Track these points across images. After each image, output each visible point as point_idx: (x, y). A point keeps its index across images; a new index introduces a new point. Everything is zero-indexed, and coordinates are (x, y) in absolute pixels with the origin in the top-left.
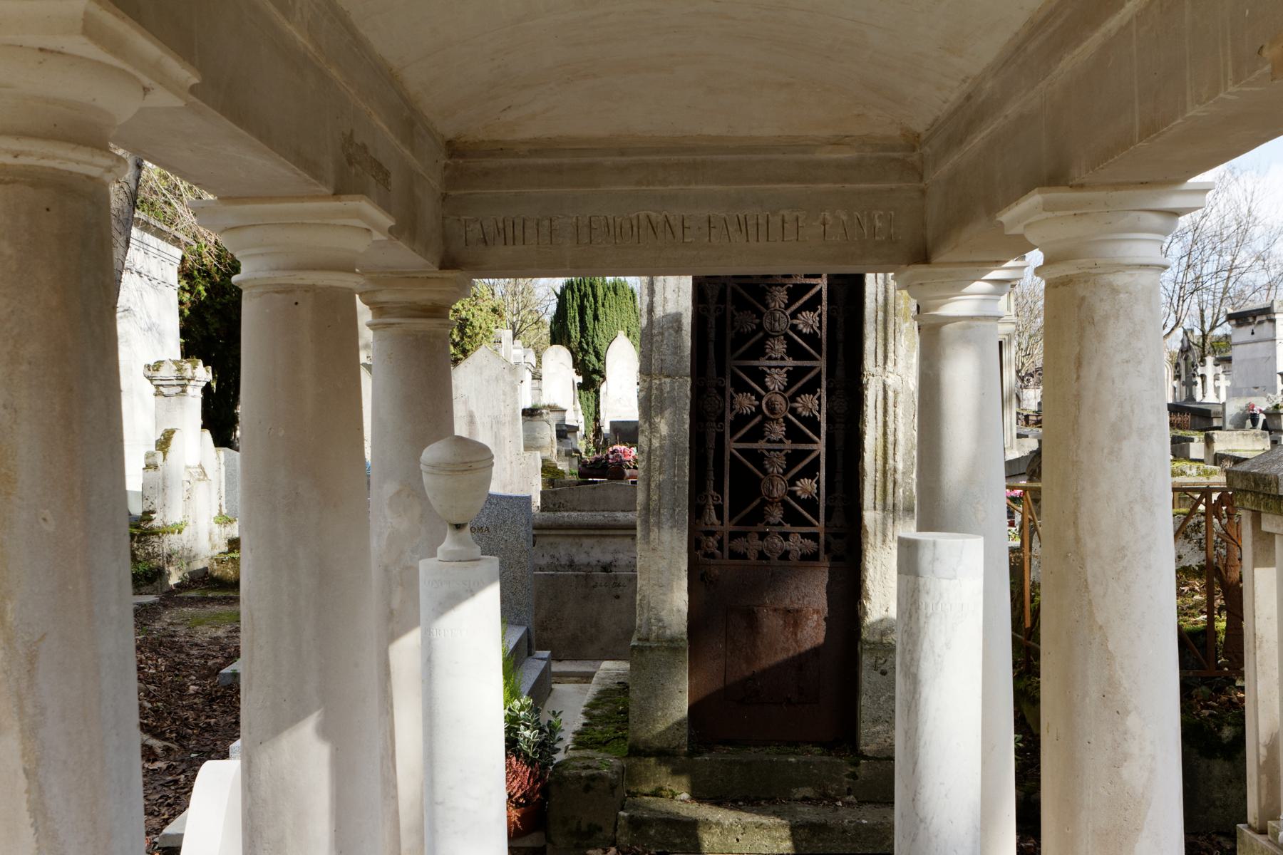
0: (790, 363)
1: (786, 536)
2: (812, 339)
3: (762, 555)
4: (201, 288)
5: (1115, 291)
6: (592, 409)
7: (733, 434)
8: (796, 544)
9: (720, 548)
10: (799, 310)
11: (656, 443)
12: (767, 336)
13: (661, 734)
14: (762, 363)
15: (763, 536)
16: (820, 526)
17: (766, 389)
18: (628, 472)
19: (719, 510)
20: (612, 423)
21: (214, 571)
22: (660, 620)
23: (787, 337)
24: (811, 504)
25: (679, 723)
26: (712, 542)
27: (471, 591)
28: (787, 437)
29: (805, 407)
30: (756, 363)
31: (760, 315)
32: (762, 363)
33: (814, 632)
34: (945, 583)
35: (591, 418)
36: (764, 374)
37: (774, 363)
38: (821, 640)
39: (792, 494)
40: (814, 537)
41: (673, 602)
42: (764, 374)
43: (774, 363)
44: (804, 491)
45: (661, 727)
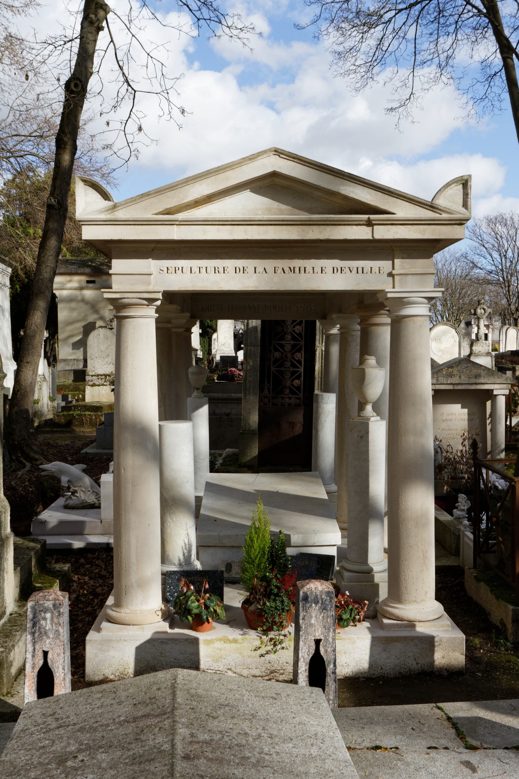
0: (292, 342)
1: (290, 398)
2: (300, 335)
3: (282, 404)
4: (18, 286)
5: (353, 336)
6: (207, 348)
7: (273, 365)
8: (293, 401)
9: (269, 402)
10: (296, 325)
11: (249, 368)
12: (285, 334)
13: (249, 460)
14: (284, 342)
15: (283, 398)
16: (301, 395)
17: (284, 350)
18: (236, 379)
19: (269, 389)
20: (221, 357)
21: (55, 420)
22: (249, 424)
23: (291, 334)
24: (298, 388)
25: (255, 457)
26: (266, 400)
27: (201, 406)
28: (291, 366)
29: (297, 357)
30: (281, 342)
31: (283, 327)
32: (284, 342)
33: (299, 429)
34: (324, 405)
35: (206, 353)
36: (284, 346)
37: (287, 342)
38: (301, 432)
39: (292, 385)
40: (299, 399)
41: (254, 419)
42: (284, 346)
43: (287, 342)
44: (296, 384)
45: (249, 458)
